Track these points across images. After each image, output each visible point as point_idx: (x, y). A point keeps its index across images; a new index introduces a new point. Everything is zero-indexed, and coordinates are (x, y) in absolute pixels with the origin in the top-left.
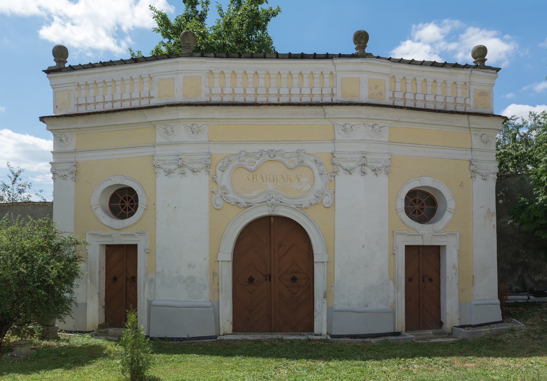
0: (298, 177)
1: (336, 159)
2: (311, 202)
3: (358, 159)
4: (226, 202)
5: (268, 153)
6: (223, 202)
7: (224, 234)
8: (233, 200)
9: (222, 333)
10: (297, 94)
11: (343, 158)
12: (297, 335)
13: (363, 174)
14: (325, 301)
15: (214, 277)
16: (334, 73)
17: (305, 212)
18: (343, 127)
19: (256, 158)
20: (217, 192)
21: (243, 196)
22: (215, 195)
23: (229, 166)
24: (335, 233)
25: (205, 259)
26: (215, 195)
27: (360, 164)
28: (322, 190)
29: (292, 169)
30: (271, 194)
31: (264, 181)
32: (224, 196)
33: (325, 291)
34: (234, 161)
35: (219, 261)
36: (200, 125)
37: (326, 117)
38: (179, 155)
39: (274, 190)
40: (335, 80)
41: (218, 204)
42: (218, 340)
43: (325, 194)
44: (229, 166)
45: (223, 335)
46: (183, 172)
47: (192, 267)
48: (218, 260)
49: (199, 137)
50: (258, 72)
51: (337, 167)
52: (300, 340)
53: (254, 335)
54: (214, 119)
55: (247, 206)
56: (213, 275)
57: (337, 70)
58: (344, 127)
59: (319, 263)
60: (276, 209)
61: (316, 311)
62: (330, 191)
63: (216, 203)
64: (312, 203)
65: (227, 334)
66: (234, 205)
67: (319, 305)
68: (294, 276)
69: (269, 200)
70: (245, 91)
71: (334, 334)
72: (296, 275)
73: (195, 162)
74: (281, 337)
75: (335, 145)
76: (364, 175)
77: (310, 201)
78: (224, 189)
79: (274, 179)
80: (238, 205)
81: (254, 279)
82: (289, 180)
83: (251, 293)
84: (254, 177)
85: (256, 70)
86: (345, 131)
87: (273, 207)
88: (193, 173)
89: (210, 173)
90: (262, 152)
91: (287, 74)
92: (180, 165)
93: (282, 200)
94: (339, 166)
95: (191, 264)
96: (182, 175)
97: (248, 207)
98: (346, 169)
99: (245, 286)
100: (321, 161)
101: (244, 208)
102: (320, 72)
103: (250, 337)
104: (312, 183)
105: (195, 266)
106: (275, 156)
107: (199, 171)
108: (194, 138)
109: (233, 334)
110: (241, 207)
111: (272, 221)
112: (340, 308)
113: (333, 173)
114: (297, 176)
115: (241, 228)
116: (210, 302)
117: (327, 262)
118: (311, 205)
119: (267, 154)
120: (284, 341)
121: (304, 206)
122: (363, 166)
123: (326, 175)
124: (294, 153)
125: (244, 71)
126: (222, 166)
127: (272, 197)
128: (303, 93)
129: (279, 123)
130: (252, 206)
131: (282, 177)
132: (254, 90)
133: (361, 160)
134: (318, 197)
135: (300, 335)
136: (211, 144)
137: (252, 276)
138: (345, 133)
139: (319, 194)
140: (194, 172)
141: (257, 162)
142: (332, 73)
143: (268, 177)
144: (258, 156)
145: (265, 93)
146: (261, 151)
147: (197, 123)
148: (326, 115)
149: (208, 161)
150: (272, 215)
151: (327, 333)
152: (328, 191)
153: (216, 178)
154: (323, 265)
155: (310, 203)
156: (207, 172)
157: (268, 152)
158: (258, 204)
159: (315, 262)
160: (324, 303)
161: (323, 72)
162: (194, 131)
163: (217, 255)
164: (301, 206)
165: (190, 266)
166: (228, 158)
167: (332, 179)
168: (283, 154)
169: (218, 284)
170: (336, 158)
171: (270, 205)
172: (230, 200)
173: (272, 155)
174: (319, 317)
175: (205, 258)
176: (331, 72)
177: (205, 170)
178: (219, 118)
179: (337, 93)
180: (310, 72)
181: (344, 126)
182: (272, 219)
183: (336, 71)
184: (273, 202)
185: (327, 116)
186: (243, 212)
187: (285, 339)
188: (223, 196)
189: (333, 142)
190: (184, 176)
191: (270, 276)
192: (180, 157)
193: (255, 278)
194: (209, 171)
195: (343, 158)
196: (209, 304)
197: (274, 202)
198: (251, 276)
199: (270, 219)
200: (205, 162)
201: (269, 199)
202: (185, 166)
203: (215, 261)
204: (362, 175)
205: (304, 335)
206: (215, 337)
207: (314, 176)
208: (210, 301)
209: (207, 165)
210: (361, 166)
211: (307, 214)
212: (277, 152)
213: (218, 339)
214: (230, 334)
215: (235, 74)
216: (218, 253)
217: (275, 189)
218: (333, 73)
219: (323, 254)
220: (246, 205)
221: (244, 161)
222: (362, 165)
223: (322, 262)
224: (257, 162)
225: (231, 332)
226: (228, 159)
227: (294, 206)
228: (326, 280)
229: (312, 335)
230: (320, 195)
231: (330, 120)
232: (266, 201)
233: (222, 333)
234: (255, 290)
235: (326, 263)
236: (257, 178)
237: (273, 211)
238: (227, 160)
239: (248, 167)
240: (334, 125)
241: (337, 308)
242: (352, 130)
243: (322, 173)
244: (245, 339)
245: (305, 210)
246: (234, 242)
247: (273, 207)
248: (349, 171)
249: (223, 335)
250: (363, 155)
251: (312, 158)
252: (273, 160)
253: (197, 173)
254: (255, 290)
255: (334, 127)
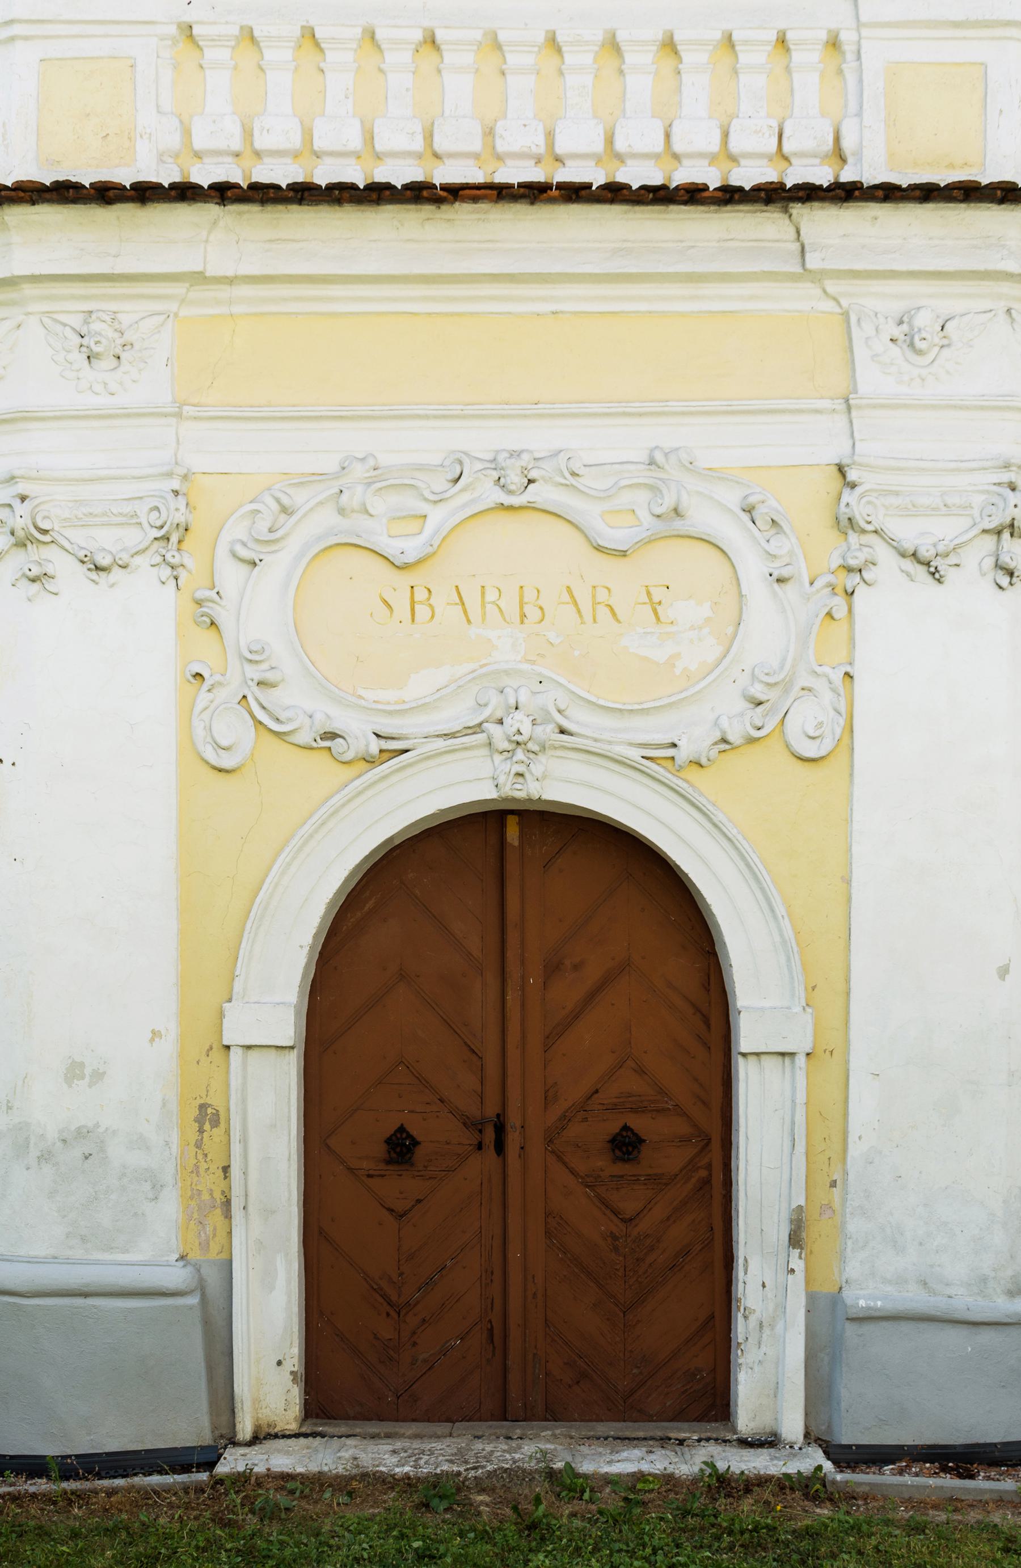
0: (656, 599)
1: (862, 497)
2: (724, 732)
3: (978, 500)
4: (271, 730)
5: (493, 466)
6: (253, 729)
7: (258, 900)
8: (307, 720)
9: (245, 1429)
10: (646, 150)
11: (897, 494)
12: (645, 1439)
13: (1004, 581)
14: (798, 1265)
15: (201, 1131)
16: (847, 37)
17: (692, 785)
18: (901, 322)
19: (427, 494)
20: (218, 678)
21: (360, 697)
22: (209, 691)
23: (282, 538)
24: (849, 900)
25: (155, 1034)
26: (209, 691)
27: (991, 526)
28: (782, 667)
29: (624, 554)
30: (507, 690)
31: (469, 621)
32: (257, 699)
33: (800, 1207)
34: (312, 509)
35: (228, 1047)
36: (125, 319)
37: (808, 266)
38: (13, 478)
39: (525, 667)
40: (851, 78)
41: (224, 743)
42: (220, 1482)
43: (797, 688)
44: (282, 538)
45: (256, 1439)
46: (36, 571)
47: (87, 1079)
48: (226, 1043)
49: (121, 384)
50: (440, 35)
51: (866, 539)
52: (668, 1479)
53: (416, 1444)
54: (198, 278)
55: (381, 751)
56: (200, 1120)
57: (863, 19)
58: (905, 327)
59: (763, 1057)
60: (537, 769)
61: (746, 1317)
62: (826, 669)
63: (215, 735)
64: (730, 738)
65: (276, 1436)
66: (312, 748)
67: (764, 1286)
68: (626, 1128)
69: (501, 722)
70: (369, 138)
71: (845, 1441)
72: (639, 1124)
73: (105, 514)
74: (568, 1464)
75: (855, 421)
76: (1011, 584)
77: (716, 723)
78: (257, 662)
79: (527, 609)
80: (330, 748)
81: (415, 1143)
82: (603, 612)
83: (402, 1216)
84: (417, 598)
85: (427, 24)
86: (912, 345)
87: (520, 755)
88: (93, 575)
89: (183, 575)
90: (461, 463)
91: (596, 48)
92: (20, 533)
93: (566, 717)
94: (874, 536)
95: (82, 1065)
96: (36, 586)
97: (386, 756)
98: (914, 555)
99: (369, 1176)
100: (778, 511)
101: (363, 765)
102: (773, 36)
103: (394, 1460)
104: (730, 630)
105: (105, 1073)
106: (530, 481)
107: (123, 567)
108: (99, 388)
109: (306, 1435)
110: (349, 756)
111: (509, 839)
112: (879, 1303)
113: (842, 574)
114: (649, 593)
115: (345, 874)
116: (181, 1263)
117: (808, 1054)
118: (723, 746)
119: (489, 472)
120: (583, 1492)
121: (683, 754)
122: (1006, 535)
123: (807, 584)
124: (632, 467)
125: (365, 30)
126: (245, 539)
127: (512, 702)
128: (678, 147)
129: (554, 307)
130: (407, 751)
131: (566, 597)
132: (419, 129)
133: (993, 501)
134: (760, 703)
135: (664, 1441)
136: (188, 418)
137: (409, 1128)
138: (910, 354)
139: (768, 684)
140: (98, 568)
141: (436, 516)
142: (834, 43)
143: (491, 596)
144: (440, 483)
145: (476, 146)
146: (459, 455)
147: (113, 306)
148: (808, 256)
149: (172, 507)
150: (514, 800)
151: (807, 1435)
152: (818, 669)
153: (213, 601)
154: (784, 1073)
155: (718, 736)
156: (168, 571)
157: (491, 461)
158: (441, 744)
159: (744, 1055)
160: (792, 1271)
161: (790, 36)
162: (96, 349)
163: (221, 1015)
164: (670, 752)
165: (74, 1072)
166: (280, 495)
167: (839, 605)
168: (574, 474)
169: (226, 1169)
170: (858, 490)
171: (506, 745)
172: (290, 720)
173: (515, 479)
174: (763, 1349)
175: (153, 1032)
176: (829, 31)
177: (158, 559)
178: (230, 273)
179: (864, 144)
180: (718, 35)
181: (905, 319)
182: (513, 831)
183: (859, 25)
184: (519, 732)
185: (813, 261)
186: (357, 783)
187: (585, 1476)
188: (250, 698)
189: (844, 406)
190: (114, 552)
191: (500, 1129)
192: (21, 488)
193: (419, 1139)
194: (175, 561)
195: (897, 494)
196: (176, 1277)
197: (526, 728)
198: (401, 1129)
199: (503, 825)
200: (155, 514)
201: (499, 714)
202: (46, 538)
203: (211, 1048)
204: (1001, 587)
205: (681, 1442)
206: (208, 1458)
207: (740, 592)
208: (182, 1258)
209: (162, 532)
210: (995, 537)
211: (701, 794)
212: (540, 464)
213: (222, 1469)
214: (289, 1437)
215: (317, 44)
216: (226, 1005)
217: (533, 662)
218: (844, 36)
219: (789, 1008)
220: (375, 746)
221: (366, 512)
222: (999, 533)
223: (783, 1054)
224: (436, 516)
225: (293, 1427)
226: (278, 501)
227: (635, 754)
228: (801, 1148)
229: (725, 1441)
230: (771, 695)
231: (830, 289)
232: (481, 724)
233: (245, 1429)
234: (419, 1201)
235: (801, 1060)
236: (432, 601)
237: (520, 780)
238: (275, 506)
239: (391, 547)
240: (846, 315)
241: (862, 1303)
242: (945, 342)
243: (785, 572)
244: (364, 1476)
245: (693, 774)
246: (312, 948)
247: (520, 755)
248: (928, 564)
249: (256, 1439)
250: (1006, 477)
251: (732, 498)
252: (521, 508)
253: (111, 575)
254: (419, 1201)
255: (849, 327)
